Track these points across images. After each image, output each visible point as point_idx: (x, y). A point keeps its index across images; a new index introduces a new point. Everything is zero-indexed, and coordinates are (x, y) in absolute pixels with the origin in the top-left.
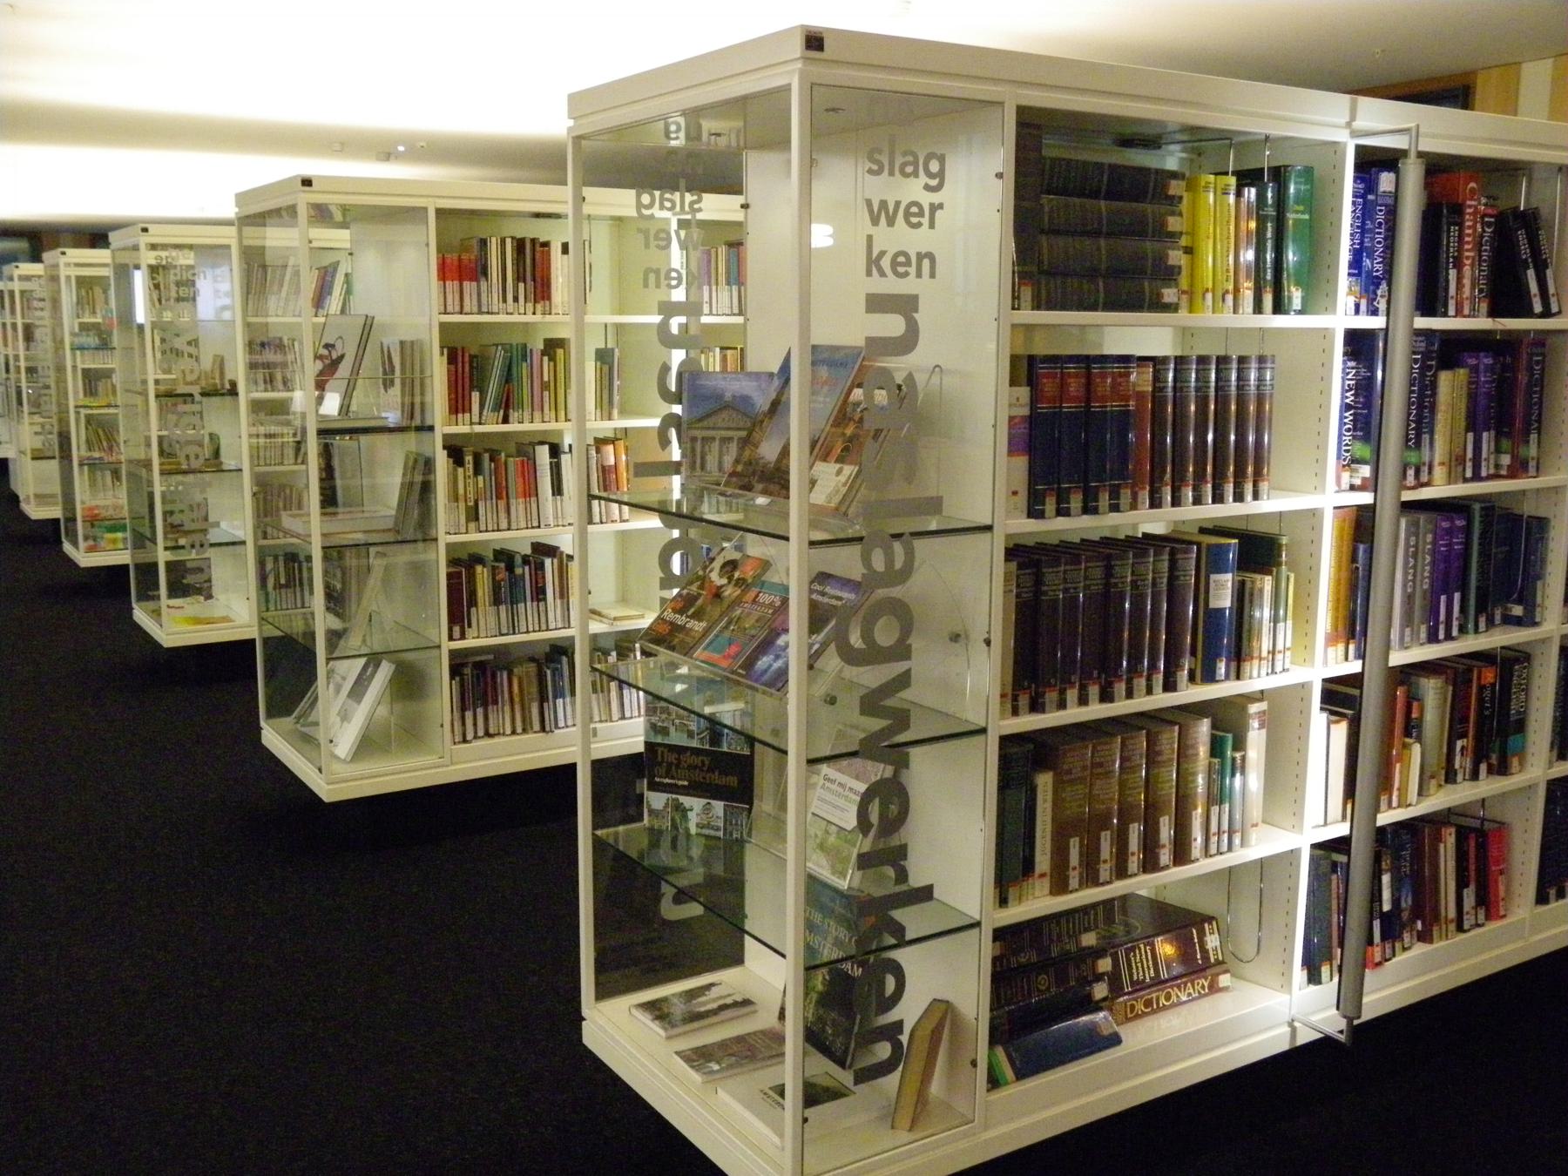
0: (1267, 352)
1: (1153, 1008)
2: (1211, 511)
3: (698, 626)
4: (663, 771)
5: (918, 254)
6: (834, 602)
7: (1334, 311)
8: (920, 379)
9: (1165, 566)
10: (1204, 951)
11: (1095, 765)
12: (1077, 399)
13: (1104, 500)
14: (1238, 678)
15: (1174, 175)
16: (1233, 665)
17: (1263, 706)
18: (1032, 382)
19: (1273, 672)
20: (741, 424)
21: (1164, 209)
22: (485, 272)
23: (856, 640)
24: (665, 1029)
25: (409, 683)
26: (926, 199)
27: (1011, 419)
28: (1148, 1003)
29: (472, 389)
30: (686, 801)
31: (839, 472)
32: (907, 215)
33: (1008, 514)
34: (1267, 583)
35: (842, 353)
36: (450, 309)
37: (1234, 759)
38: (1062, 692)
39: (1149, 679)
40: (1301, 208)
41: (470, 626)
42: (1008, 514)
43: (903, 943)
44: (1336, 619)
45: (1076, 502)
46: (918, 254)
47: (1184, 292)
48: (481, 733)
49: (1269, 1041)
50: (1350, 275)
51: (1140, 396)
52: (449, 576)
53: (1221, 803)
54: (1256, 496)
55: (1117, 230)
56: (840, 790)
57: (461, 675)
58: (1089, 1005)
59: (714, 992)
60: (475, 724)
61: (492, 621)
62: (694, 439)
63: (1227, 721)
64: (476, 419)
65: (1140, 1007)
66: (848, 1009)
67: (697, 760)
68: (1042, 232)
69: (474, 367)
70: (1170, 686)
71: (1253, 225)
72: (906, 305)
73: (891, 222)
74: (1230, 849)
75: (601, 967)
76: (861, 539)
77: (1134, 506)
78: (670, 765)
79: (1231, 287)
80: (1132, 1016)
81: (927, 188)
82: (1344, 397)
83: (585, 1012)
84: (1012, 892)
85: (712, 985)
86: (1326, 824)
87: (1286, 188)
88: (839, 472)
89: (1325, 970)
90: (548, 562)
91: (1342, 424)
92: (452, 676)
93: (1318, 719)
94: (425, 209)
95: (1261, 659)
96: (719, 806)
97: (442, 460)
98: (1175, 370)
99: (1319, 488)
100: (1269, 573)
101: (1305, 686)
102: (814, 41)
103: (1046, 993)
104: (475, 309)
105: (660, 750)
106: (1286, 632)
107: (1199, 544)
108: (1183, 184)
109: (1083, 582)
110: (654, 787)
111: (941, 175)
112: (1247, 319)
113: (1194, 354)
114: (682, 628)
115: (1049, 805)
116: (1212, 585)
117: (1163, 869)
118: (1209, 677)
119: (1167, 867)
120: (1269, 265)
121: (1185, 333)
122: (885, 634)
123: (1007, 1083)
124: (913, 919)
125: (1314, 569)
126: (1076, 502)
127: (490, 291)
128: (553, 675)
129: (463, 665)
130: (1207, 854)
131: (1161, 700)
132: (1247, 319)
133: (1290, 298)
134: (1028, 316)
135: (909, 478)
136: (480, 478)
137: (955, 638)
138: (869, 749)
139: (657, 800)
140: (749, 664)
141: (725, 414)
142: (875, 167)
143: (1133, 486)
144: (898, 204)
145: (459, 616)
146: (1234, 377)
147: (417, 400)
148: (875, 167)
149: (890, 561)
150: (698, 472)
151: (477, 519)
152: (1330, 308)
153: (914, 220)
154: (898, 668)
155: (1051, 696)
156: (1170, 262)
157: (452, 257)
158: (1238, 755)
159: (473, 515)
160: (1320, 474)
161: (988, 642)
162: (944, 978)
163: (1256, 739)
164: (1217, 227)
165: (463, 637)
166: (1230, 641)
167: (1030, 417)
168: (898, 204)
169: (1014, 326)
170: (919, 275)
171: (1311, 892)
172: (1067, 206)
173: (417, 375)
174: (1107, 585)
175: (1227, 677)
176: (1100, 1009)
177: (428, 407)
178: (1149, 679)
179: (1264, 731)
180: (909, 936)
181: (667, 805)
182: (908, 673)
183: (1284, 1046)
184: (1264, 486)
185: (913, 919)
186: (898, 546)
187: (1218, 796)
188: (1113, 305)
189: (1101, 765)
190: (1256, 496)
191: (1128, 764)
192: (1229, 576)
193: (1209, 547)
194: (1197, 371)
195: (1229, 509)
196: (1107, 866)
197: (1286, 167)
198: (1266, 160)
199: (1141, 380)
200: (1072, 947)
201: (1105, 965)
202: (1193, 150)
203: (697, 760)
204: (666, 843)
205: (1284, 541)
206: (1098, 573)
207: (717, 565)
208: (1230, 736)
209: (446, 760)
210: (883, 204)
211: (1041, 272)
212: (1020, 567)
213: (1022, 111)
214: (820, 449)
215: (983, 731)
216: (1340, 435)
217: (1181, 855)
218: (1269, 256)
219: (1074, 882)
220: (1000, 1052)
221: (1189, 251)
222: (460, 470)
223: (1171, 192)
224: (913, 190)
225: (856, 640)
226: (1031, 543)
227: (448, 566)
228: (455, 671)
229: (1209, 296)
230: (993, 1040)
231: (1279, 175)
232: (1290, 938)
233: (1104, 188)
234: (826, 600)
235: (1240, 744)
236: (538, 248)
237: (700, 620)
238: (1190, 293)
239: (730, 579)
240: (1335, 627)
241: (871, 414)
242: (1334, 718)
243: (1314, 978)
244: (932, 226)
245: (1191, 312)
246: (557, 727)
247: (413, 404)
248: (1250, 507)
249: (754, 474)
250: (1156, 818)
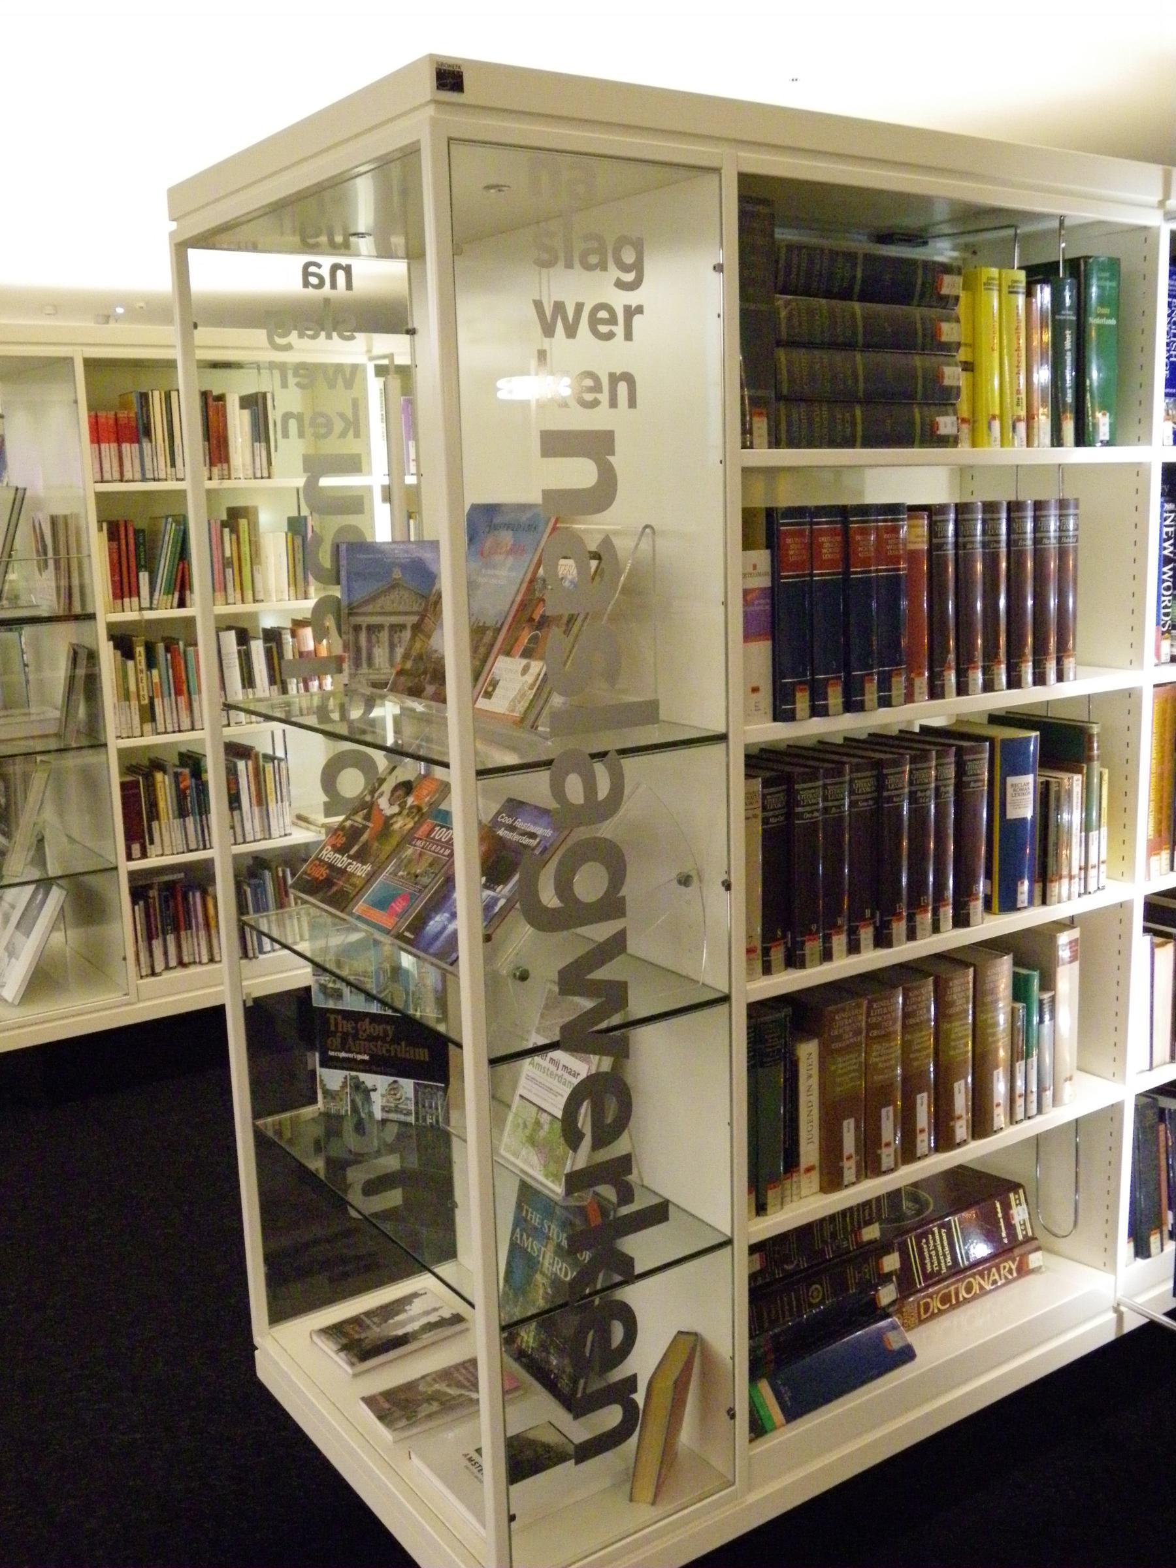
0: (1069, 495)
1: (950, 1303)
2: (1005, 699)
3: (361, 870)
4: (337, 1041)
5: (612, 376)
6: (525, 841)
7: (1149, 442)
8: (623, 545)
9: (951, 772)
10: (1010, 1227)
11: (870, 1027)
12: (832, 563)
13: (871, 693)
14: (1044, 902)
15: (946, 269)
16: (1038, 887)
17: (1075, 933)
18: (773, 542)
19: (1086, 892)
20: (415, 609)
21: (934, 313)
22: (147, 432)
23: (549, 898)
24: (352, 1364)
25: (86, 905)
26: (620, 300)
27: (746, 592)
28: (945, 1299)
29: (139, 568)
30: (369, 1079)
31: (525, 670)
32: (594, 322)
33: (748, 717)
34: (1076, 782)
35: (529, 514)
36: (107, 476)
37: (1041, 1002)
38: (827, 939)
39: (936, 912)
40: (1106, 311)
41: (152, 842)
42: (748, 717)
43: (631, 1277)
44: (1159, 822)
45: (835, 698)
46: (612, 376)
47: (964, 421)
48: (173, 963)
49: (1091, 1332)
50: (1167, 395)
51: (913, 556)
52: (124, 786)
53: (1028, 1055)
54: (1060, 678)
55: (879, 340)
56: (553, 1068)
57: (146, 899)
58: (874, 1312)
59: (416, 1307)
60: (166, 953)
61: (178, 836)
62: (357, 629)
63: (1031, 955)
64: (145, 603)
65: (936, 1304)
66: (570, 1339)
67: (379, 1029)
68: (779, 343)
69: (140, 544)
70: (962, 920)
71: (1047, 337)
72: (598, 446)
73: (571, 332)
74: (1040, 1111)
76: (548, 764)
77: (909, 698)
78: (345, 1036)
79: (1023, 413)
80: (927, 1315)
81: (620, 285)
82: (1162, 548)
83: (257, 1340)
84: (772, 1196)
85: (415, 1295)
86: (1151, 1068)
87: (1088, 286)
88: (525, 670)
89: (1154, 1240)
90: (241, 765)
91: (1161, 581)
93: (1141, 942)
94: (70, 360)
95: (1071, 877)
96: (407, 1085)
97: (107, 653)
98: (956, 522)
99: (1136, 661)
100: (1080, 772)
101: (1123, 907)
102: (449, 78)
103: (819, 1312)
104: (138, 476)
105: (332, 1017)
106: (1100, 840)
107: (992, 741)
108: (959, 280)
109: (849, 796)
110: (327, 1062)
111: (638, 267)
112: (1044, 454)
113: (978, 499)
114: (343, 872)
115: (815, 1081)
116: (1009, 791)
117: (959, 1145)
118: (1009, 904)
119: (965, 1142)
120: (1069, 383)
121: (964, 472)
122: (590, 884)
123: (775, 1428)
124: (642, 1247)
125: (1132, 762)
126: (835, 698)
127: (154, 454)
128: (255, 894)
129: (149, 887)
130: (1012, 1121)
131: (952, 938)
132: (1044, 454)
133: (1095, 425)
134: (764, 456)
135: (612, 675)
136: (155, 672)
137: (685, 881)
138: (573, 1039)
139: (333, 1078)
140: (419, 924)
141: (395, 595)
142: (545, 256)
143: (910, 670)
144: (579, 307)
145: (138, 833)
146: (1029, 526)
147: (76, 582)
148: (545, 256)
149: (590, 787)
150: (364, 669)
151: (153, 719)
152: (1144, 438)
153: (604, 329)
154: (601, 932)
155: (813, 947)
156: (947, 382)
157: (106, 416)
158: (1046, 996)
159: (149, 714)
160: (1136, 646)
161: (727, 886)
162: (688, 1310)
163: (1067, 980)
164: (1001, 333)
165: (144, 855)
166: (1032, 856)
167: (772, 588)
168: (579, 307)
169: (747, 471)
170: (613, 403)
171: (1138, 1146)
172: (811, 313)
173: (74, 554)
174: (878, 800)
175: (1031, 902)
176: (888, 1316)
177: (88, 591)
178: (936, 912)
179: (1076, 964)
180: (638, 1270)
181: (345, 1083)
182: (622, 935)
183: (1109, 1336)
184: (1070, 664)
185: (642, 1247)
186: (600, 769)
187: (1024, 1044)
188: (870, 441)
189: (877, 1026)
190: (1060, 678)
191: (912, 1021)
192: (1030, 778)
193: (1006, 743)
194: (984, 522)
195: (1028, 696)
196: (891, 1150)
197: (1086, 258)
198: (1062, 251)
199: (914, 535)
200: (849, 1244)
201: (891, 1262)
202: (966, 247)
203: (379, 1029)
204: (348, 1126)
205: (1095, 729)
206: (865, 785)
207: (387, 787)
208: (1036, 974)
209: (132, 997)
210: (559, 307)
211: (779, 398)
212: (766, 784)
213: (746, 181)
214: (485, 644)
215: (725, 999)
216: (1159, 595)
217: (981, 1126)
218: (1069, 375)
219: (849, 1174)
220: (764, 1387)
221: (968, 367)
222: (130, 663)
223: (945, 291)
224: (600, 289)
225: (549, 898)
226: (783, 746)
227: (122, 774)
228: (138, 893)
229: (996, 424)
230: (756, 1371)
231: (1077, 268)
232: (1113, 1207)
233: (857, 288)
234: (514, 837)
235: (1048, 983)
236: (210, 401)
237: (364, 863)
238: (971, 422)
239: (402, 806)
240: (1159, 832)
241: (557, 591)
242: (1158, 940)
243: (1142, 1250)
244: (628, 336)
245: (974, 444)
246: (261, 952)
247: (70, 588)
248: (1054, 691)
249: (425, 673)
250: (948, 1082)
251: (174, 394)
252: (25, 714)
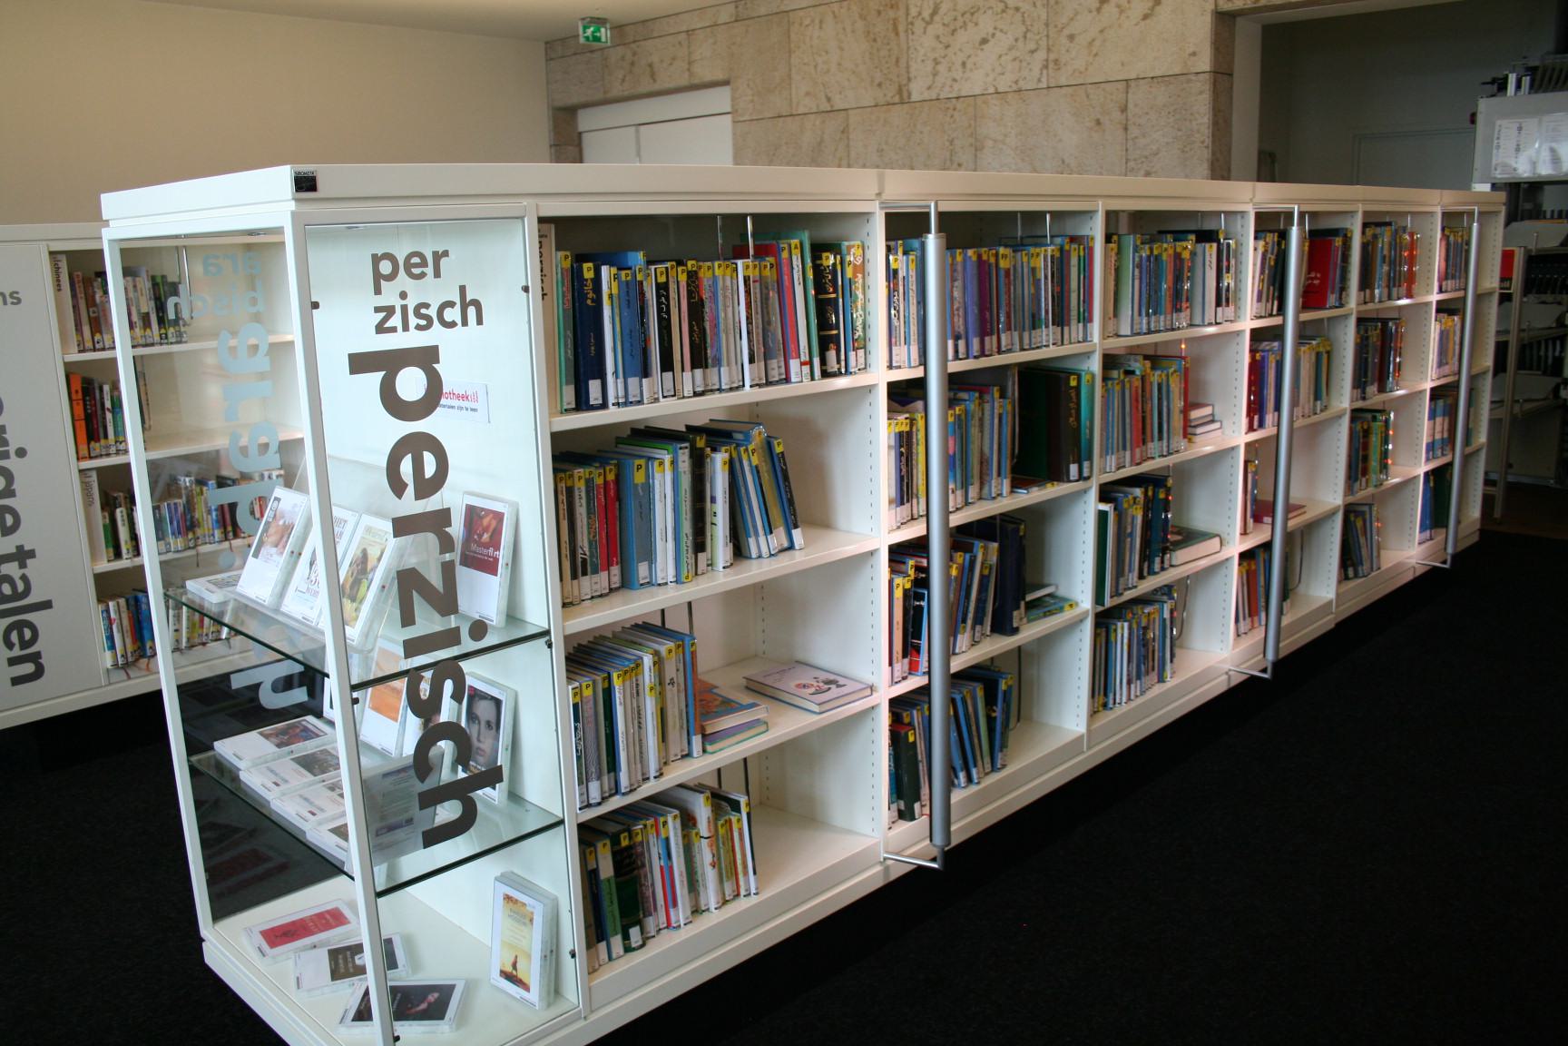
75: (214, 876)
83: (204, 932)
92: (103, 509)
170: (13, 662)
244: (437, 274)
251: (763, 728)
252: (984, 462)
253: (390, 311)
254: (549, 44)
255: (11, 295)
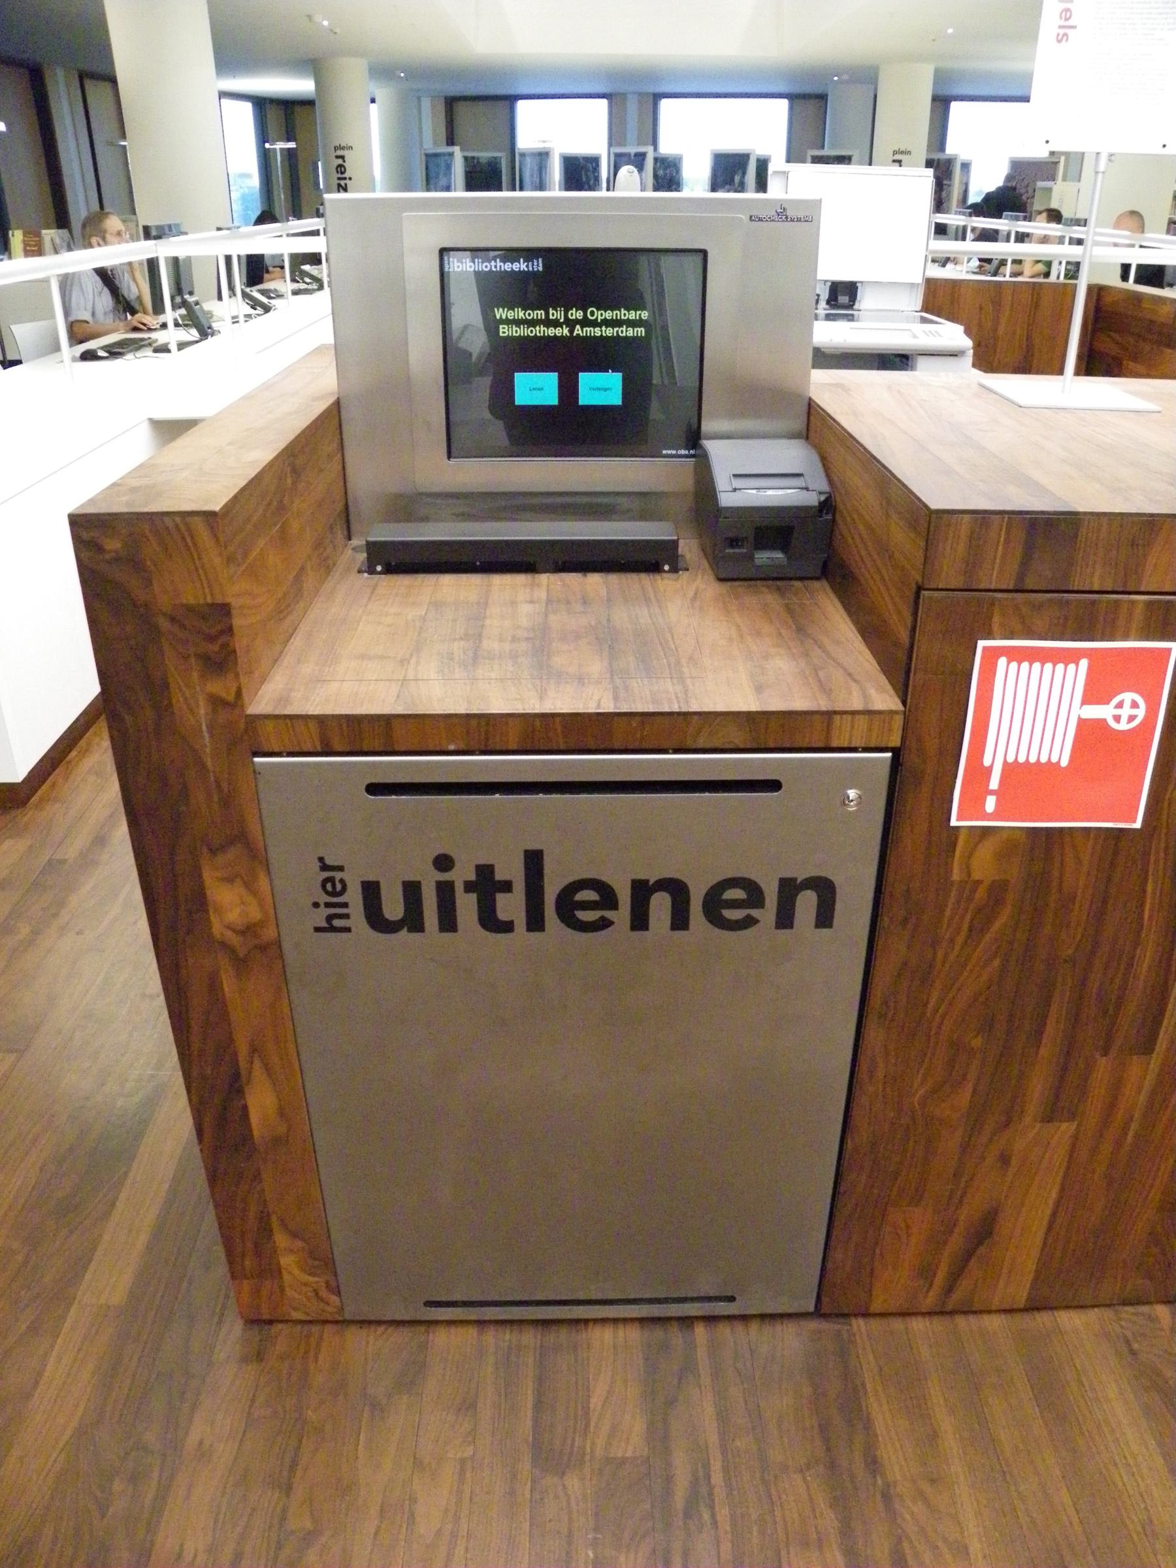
83: (523, 914)
244: (341, 869)
253: (339, 185)
254: (451, 103)
255: (1065, 35)
